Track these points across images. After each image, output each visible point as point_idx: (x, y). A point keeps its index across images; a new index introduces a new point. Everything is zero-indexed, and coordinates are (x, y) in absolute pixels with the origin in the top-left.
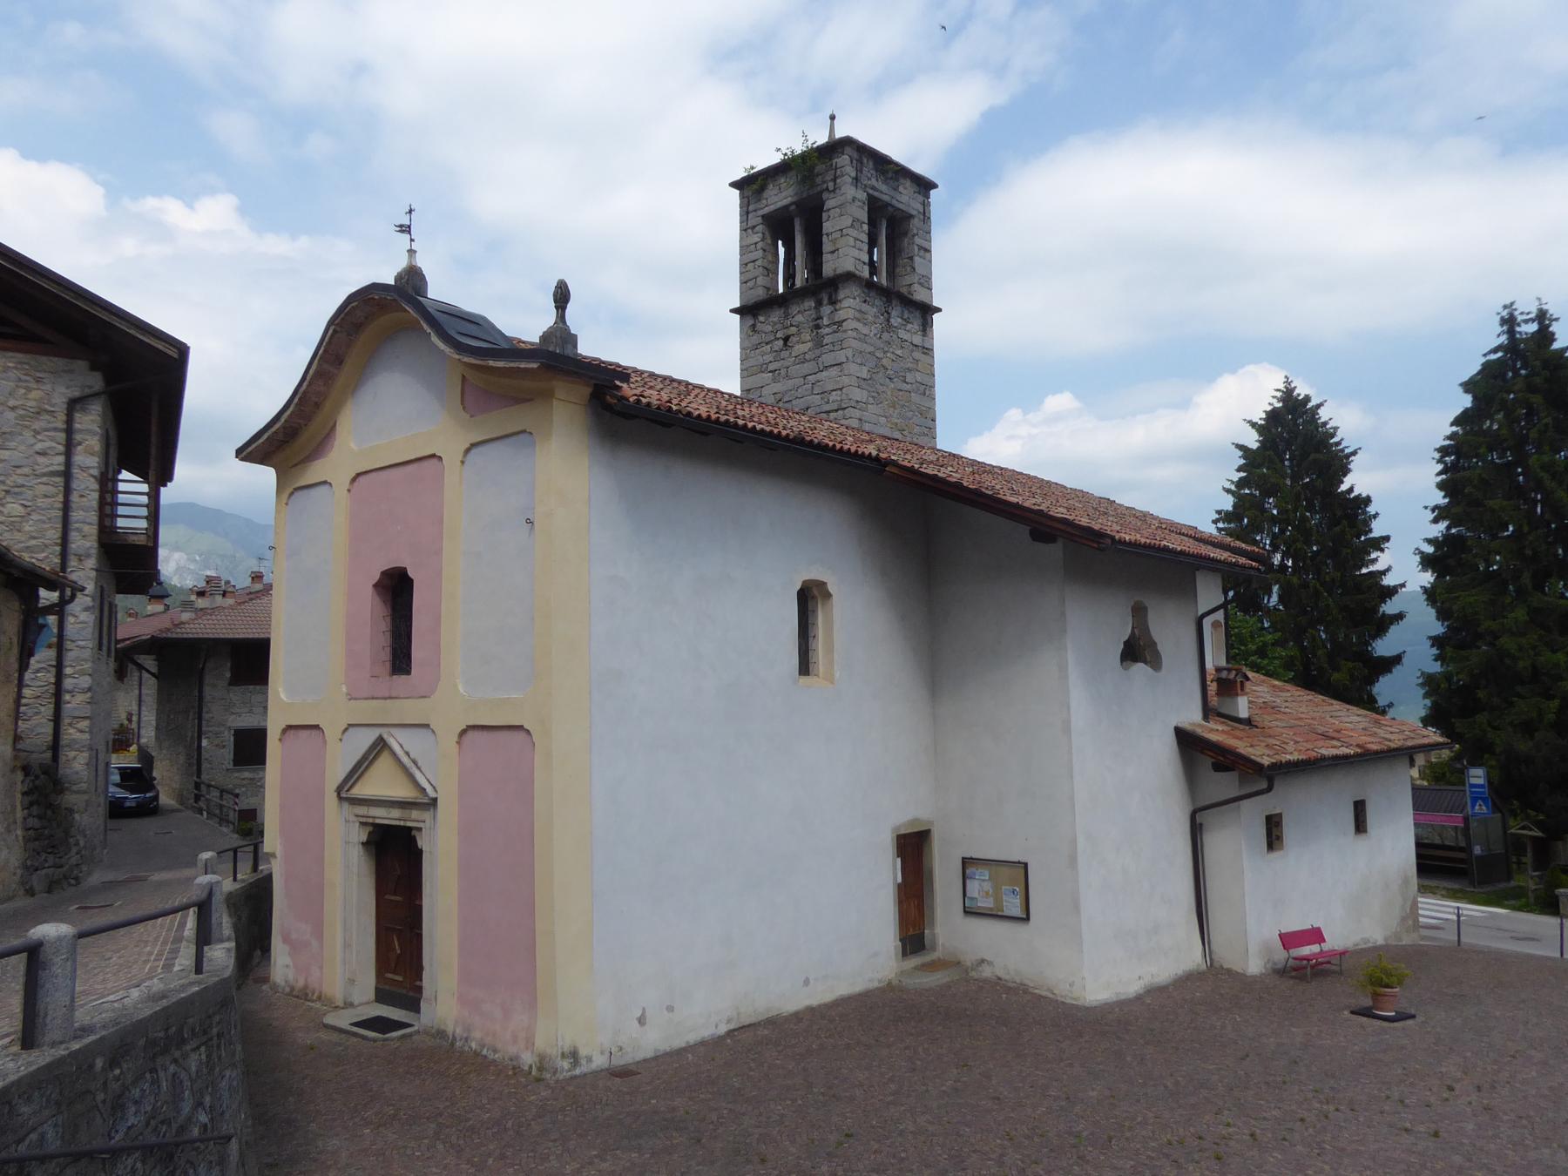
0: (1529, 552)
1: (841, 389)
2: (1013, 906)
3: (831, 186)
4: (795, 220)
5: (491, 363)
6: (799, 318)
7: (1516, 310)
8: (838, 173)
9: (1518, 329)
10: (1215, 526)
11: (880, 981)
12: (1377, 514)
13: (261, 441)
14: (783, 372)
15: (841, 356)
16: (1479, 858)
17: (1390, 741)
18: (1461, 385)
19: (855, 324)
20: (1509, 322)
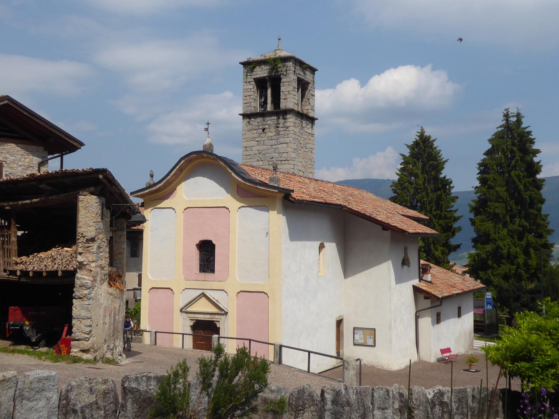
0: (509, 208)
1: (287, 153)
2: (370, 342)
3: (285, 73)
4: (268, 82)
5: (258, 187)
6: (270, 122)
7: (509, 111)
8: (288, 68)
9: (510, 119)
10: (391, 188)
11: (333, 366)
12: (453, 186)
13: (145, 192)
14: (262, 142)
15: (287, 140)
16: (488, 325)
17: (469, 287)
18: (488, 140)
19: (294, 128)
20: (507, 116)
